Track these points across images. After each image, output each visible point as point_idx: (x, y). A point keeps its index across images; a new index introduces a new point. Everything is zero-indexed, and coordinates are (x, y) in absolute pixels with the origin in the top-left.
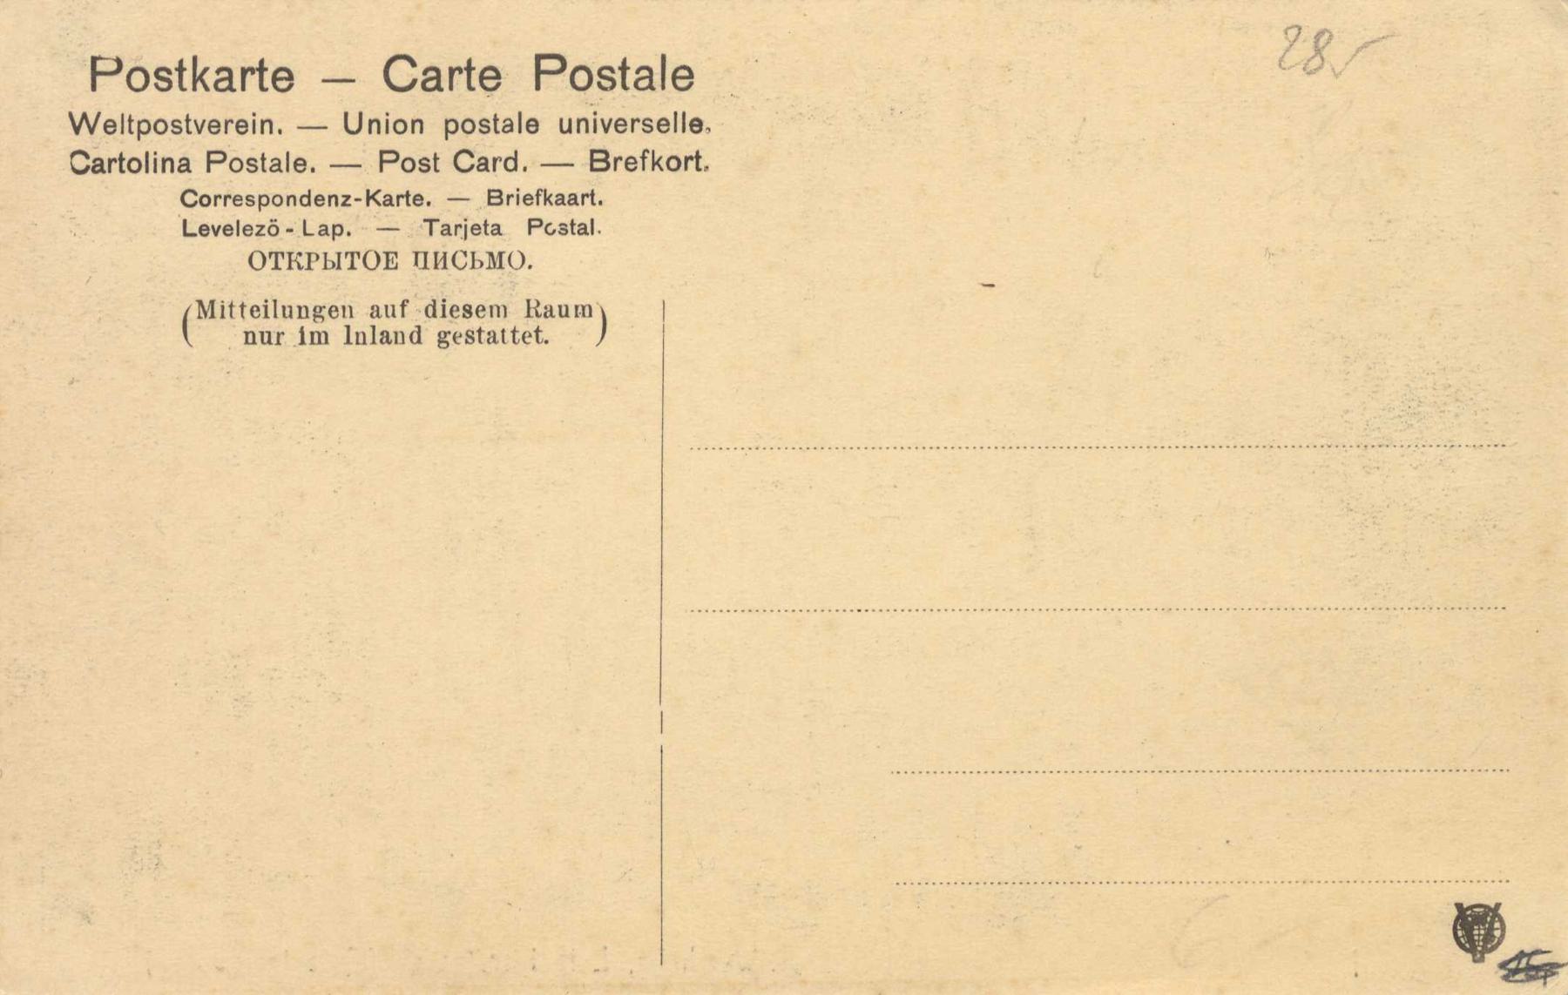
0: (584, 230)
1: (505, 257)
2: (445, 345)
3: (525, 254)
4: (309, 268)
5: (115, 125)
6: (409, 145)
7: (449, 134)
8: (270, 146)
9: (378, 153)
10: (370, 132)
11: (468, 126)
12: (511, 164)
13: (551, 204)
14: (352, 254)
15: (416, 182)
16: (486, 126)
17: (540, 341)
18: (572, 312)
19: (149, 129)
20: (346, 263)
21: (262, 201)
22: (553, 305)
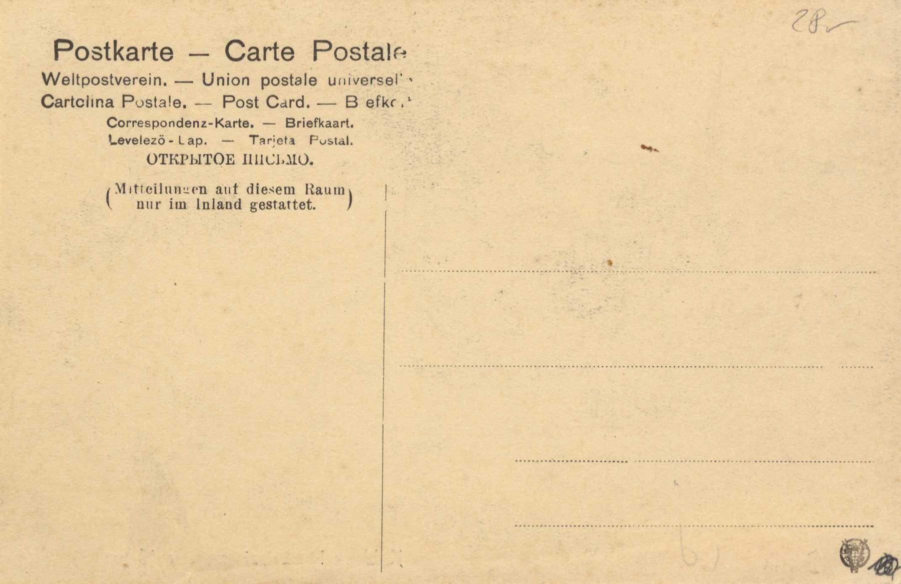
0: (345, 142)
1: (297, 157)
2: (255, 210)
3: (309, 157)
4: (182, 163)
5: (69, 80)
6: (242, 92)
7: (264, 86)
8: (160, 93)
9: (223, 97)
10: (218, 84)
11: (275, 82)
12: (300, 103)
13: (323, 126)
14: (208, 155)
15: (245, 114)
16: (106, 81)
17: (310, 208)
18: (332, 191)
19: (272, 80)
20: (204, 160)
21: (155, 124)
22: (221, 187)
